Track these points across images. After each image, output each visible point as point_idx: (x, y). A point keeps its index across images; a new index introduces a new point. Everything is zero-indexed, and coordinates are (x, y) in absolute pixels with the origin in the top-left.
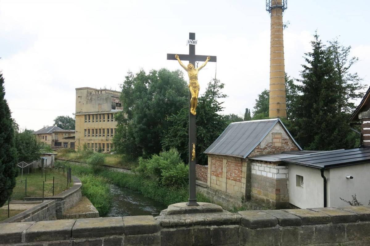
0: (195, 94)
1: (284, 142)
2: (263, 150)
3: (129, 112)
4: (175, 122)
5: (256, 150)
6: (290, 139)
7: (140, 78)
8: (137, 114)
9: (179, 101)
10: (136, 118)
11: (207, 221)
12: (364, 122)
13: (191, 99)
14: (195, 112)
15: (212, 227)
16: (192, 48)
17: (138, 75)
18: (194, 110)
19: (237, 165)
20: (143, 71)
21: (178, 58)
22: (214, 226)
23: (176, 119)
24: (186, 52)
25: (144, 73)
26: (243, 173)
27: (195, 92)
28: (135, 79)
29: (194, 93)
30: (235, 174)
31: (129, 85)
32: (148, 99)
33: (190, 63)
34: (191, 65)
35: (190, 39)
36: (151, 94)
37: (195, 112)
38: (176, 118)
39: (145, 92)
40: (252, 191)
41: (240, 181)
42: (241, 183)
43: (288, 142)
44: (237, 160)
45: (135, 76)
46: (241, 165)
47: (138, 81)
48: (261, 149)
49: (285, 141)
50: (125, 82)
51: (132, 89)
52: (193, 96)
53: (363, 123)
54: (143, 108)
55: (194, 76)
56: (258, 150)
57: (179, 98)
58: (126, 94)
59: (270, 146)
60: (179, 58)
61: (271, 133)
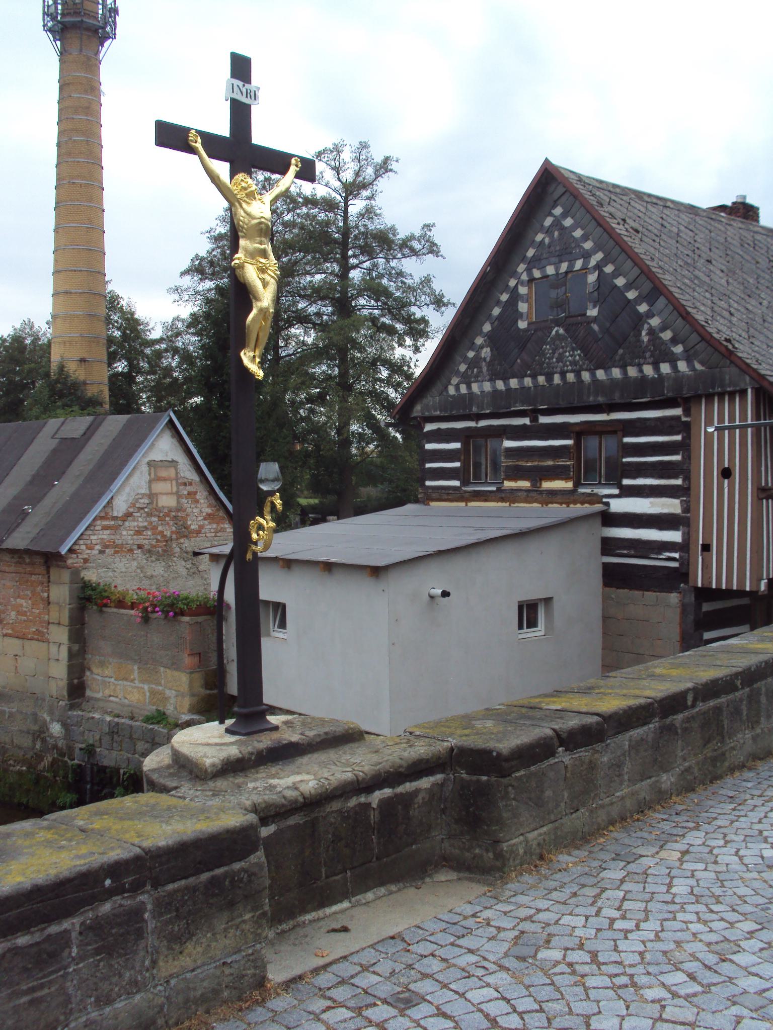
1: (186, 492)
2: (120, 523)
5: (99, 522)
6: (201, 481)
11: (364, 779)
12: (429, 427)
15: (377, 797)
19: (27, 581)
22: (382, 792)
24: (222, 127)
26: (54, 609)
30: (19, 613)
40: (89, 669)
41: (40, 637)
42: (45, 645)
43: (196, 493)
44: (27, 560)
46: (45, 580)
48: (115, 518)
49: (189, 488)
53: (425, 430)
56: (106, 523)
59: (143, 508)
61: (147, 460)
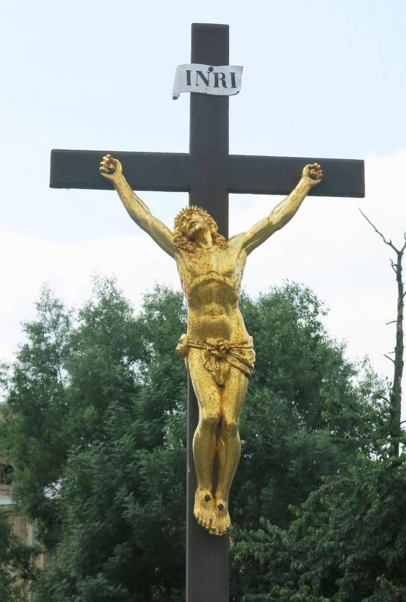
0: (222, 400)
3: (48, 517)
4: (278, 567)
7: (99, 332)
8: (82, 519)
9: (303, 450)
10: (72, 543)
13: (198, 430)
14: (220, 516)
16: (210, 115)
17: (88, 315)
18: (220, 502)
20: (114, 294)
21: (118, 178)
23: (282, 547)
24: (175, 139)
25: (123, 306)
27: (221, 387)
28: (75, 340)
29: (214, 388)
31: (43, 370)
32: (139, 444)
33: (192, 202)
34: (195, 217)
35: (196, 59)
36: (159, 414)
37: (220, 516)
38: (285, 540)
39: (126, 402)
45: (77, 324)
47: (91, 350)
50: (25, 355)
51: (62, 393)
52: (203, 414)
54: (111, 492)
55: (211, 280)
57: (300, 435)
58: (26, 413)
60: (124, 173)
